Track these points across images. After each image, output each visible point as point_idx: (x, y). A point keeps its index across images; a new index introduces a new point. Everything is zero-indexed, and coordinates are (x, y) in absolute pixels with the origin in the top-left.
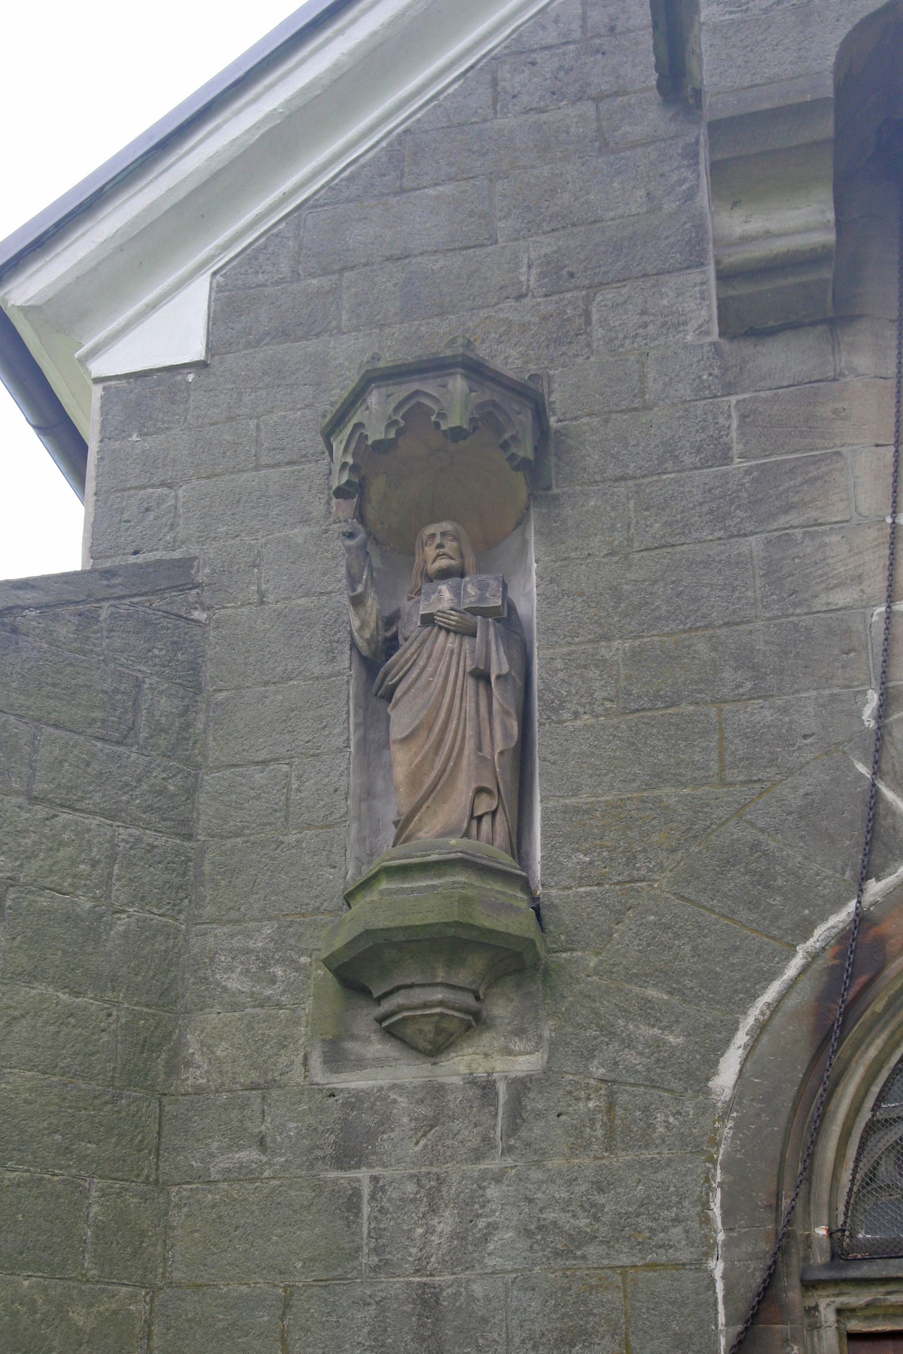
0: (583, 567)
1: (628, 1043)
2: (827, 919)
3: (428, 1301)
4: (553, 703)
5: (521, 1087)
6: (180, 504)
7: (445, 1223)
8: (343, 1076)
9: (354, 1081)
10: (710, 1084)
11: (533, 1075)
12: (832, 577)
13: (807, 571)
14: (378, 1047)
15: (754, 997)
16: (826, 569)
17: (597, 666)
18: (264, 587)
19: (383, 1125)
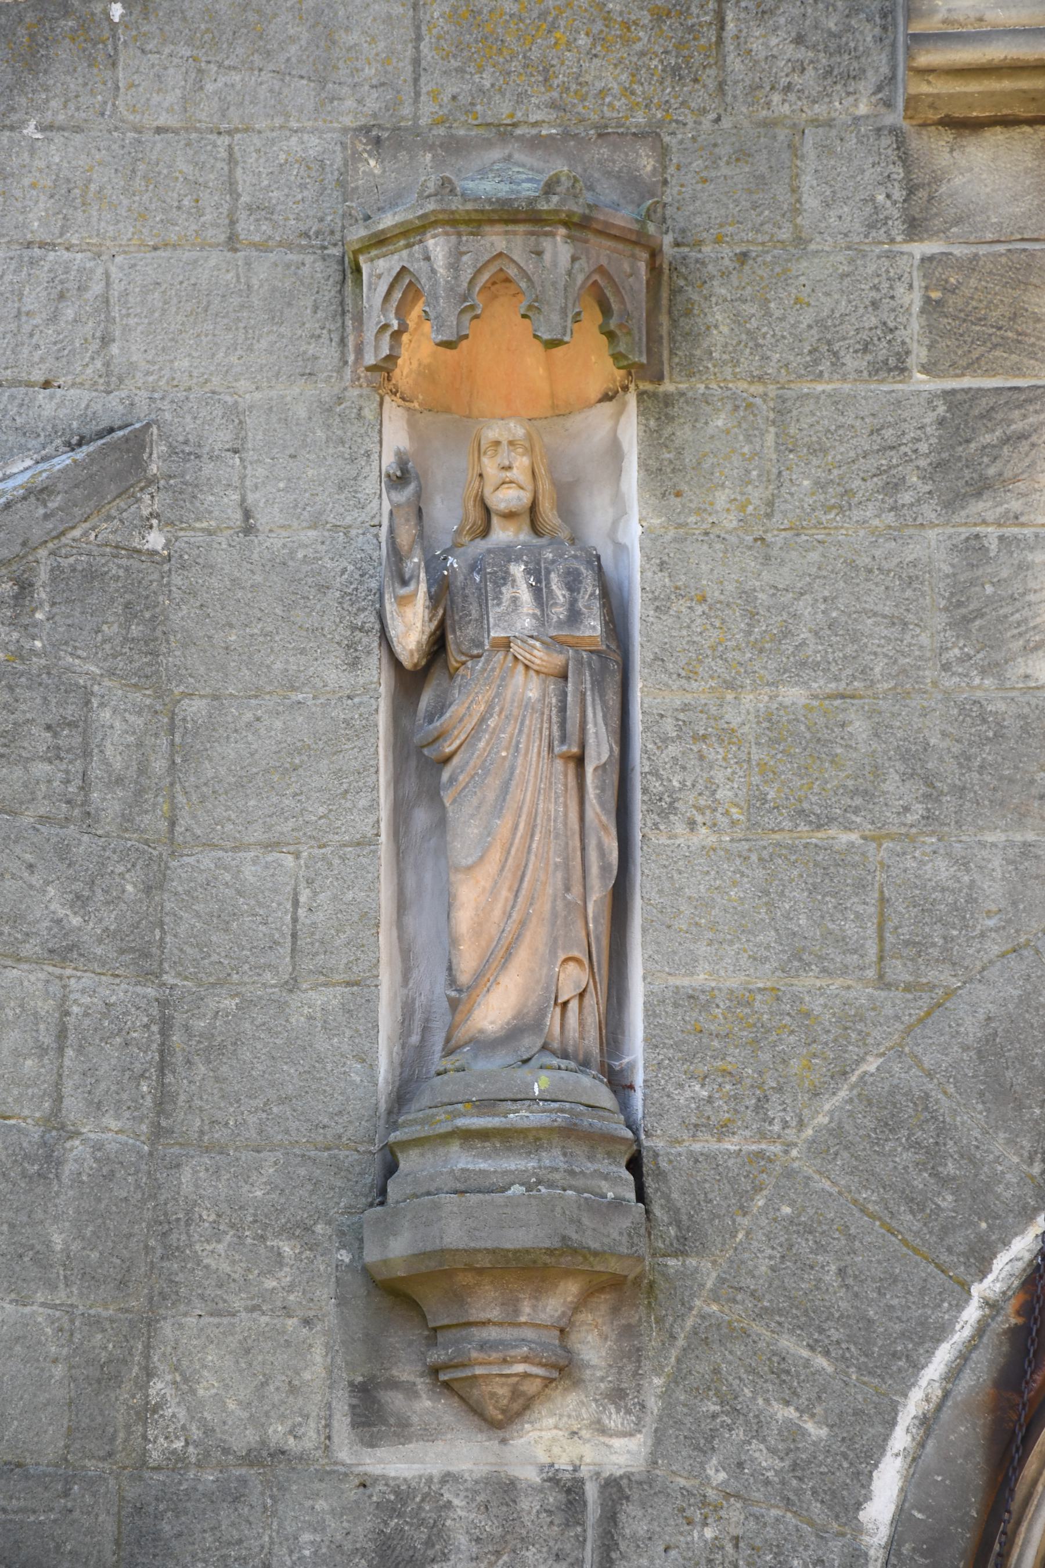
0: (705, 547)
1: (758, 1430)
2: (1010, 1243)
4: (660, 800)
5: (616, 1489)
6: (114, 294)
8: (381, 1452)
9: (396, 1464)
10: (862, 1516)
11: (632, 1474)
12: (1034, 628)
13: (1001, 612)
14: (426, 1405)
15: (917, 1367)
16: (1026, 612)
17: (721, 741)
18: (250, 498)
19: (433, 1546)
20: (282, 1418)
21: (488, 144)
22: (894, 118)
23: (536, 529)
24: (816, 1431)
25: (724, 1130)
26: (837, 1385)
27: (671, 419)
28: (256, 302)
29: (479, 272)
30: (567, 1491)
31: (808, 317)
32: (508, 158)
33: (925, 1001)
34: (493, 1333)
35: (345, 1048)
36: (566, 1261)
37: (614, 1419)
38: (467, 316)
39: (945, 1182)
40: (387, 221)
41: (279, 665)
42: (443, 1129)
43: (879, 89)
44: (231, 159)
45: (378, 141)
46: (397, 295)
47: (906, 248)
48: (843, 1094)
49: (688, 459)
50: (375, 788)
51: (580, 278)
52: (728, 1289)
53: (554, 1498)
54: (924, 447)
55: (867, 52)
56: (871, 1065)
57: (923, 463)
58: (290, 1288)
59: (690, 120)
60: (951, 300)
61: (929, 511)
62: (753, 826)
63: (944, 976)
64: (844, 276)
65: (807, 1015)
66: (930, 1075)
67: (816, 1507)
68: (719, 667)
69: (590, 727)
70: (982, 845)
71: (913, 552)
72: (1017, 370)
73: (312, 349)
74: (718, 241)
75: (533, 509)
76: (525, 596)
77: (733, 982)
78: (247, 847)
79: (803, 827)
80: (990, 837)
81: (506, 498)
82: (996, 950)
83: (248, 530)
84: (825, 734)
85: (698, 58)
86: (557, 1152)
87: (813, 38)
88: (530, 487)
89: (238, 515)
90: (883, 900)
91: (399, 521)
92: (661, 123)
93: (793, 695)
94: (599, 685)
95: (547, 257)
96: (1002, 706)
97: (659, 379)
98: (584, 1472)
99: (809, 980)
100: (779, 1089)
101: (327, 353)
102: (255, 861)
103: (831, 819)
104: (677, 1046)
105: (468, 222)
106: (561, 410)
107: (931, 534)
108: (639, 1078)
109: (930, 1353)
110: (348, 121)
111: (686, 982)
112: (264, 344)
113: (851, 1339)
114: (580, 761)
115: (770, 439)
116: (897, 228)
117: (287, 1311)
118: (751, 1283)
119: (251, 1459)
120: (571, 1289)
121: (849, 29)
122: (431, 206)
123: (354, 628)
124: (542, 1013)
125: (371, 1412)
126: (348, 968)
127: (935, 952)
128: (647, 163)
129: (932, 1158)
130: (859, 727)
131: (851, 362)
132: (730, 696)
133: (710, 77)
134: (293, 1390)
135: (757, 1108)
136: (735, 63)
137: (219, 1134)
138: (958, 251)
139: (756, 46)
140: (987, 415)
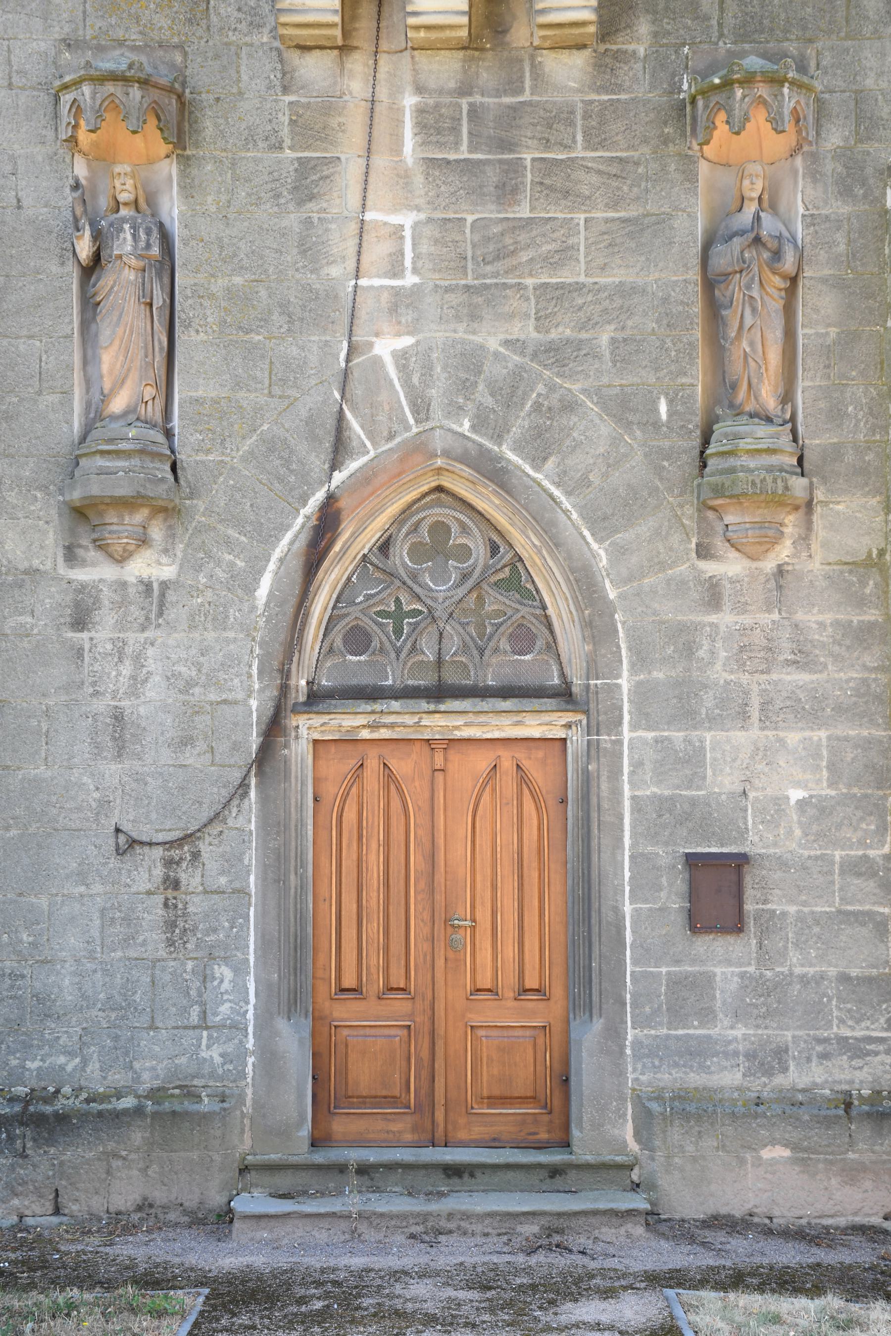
1: (218, 563)
3: (118, 717)
5: (165, 585)
7: (127, 669)
9: (81, 575)
14: (92, 554)
15: (279, 540)
18: (20, 194)
20: (38, 558)
21: (114, 48)
22: (277, 44)
23: (137, 210)
24: (240, 564)
25: (208, 452)
26: (249, 547)
27: (189, 166)
28: (20, 111)
29: (103, 101)
30: (147, 586)
31: (243, 126)
32: (122, 55)
33: (286, 403)
34: (115, 528)
35: (61, 418)
36: (139, 501)
37: (164, 560)
38: (99, 120)
39: (292, 471)
40: (67, 79)
41: (32, 264)
42: (94, 450)
43: (271, 32)
44: (9, 51)
45: (69, 45)
46: (74, 110)
47: (282, 98)
48: (254, 438)
49: (196, 182)
50: (72, 315)
51: (145, 106)
52: (209, 512)
53: (141, 588)
54: (289, 180)
55: (266, 16)
56: (265, 427)
57: (289, 187)
58: (40, 510)
59: (196, 41)
60: (300, 120)
61: (291, 207)
62: (221, 332)
63: (293, 393)
64: (258, 109)
65: (241, 407)
66: (287, 431)
67: (240, 591)
68: (208, 268)
69: (155, 292)
70: (310, 341)
71: (285, 223)
72: (325, 150)
73: (44, 132)
74: (208, 92)
75: (136, 201)
76: (129, 237)
77: (213, 394)
78: (21, 337)
79: (241, 333)
80: (313, 338)
81: (123, 197)
82: (314, 382)
83: (19, 207)
84: (250, 296)
85: (199, 15)
86: (137, 459)
87: (245, 9)
88: (134, 192)
89: (15, 201)
90: (271, 363)
91: (76, 205)
92: (184, 42)
93: (238, 280)
94: (159, 275)
95: (131, 95)
96: (318, 286)
97: (185, 149)
98: (153, 579)
99: (242, 394)
100: (230, 436)
101: (50, 134)
102: (24, 343)
103: (252, 330)
104: (190, 419)
105: (98, 80)
106: (151, 162)
107: (292, 216)
108: (176, 431)
109: (284, 535)
110: (57, 36)
111: (194, 394)
112: (24, 129)
113: (254, 530)
114: (151, 305)
115: (229, 175)
116: (279, 89)
117: (39, 518)
118: (217, 509)
119: (26, 572)
120: (145, 512)
121: (259, 6)
122: (82, 72)
123: (62, 249)
124: (137, 405)
125: (71, 555)
126: (62, 387)
127: (290, 383)
128: (178, 58)
129: (287, 462)
130: (263, 293)
131: (261, 144)
132: (213, 280)
133: (204, 23)
134: (42, 547)
135: (221, 443)
136: (214, 19)
137: (12, 451)
138: (303, 100)
139: (222, 11)
140: (314, 168)
